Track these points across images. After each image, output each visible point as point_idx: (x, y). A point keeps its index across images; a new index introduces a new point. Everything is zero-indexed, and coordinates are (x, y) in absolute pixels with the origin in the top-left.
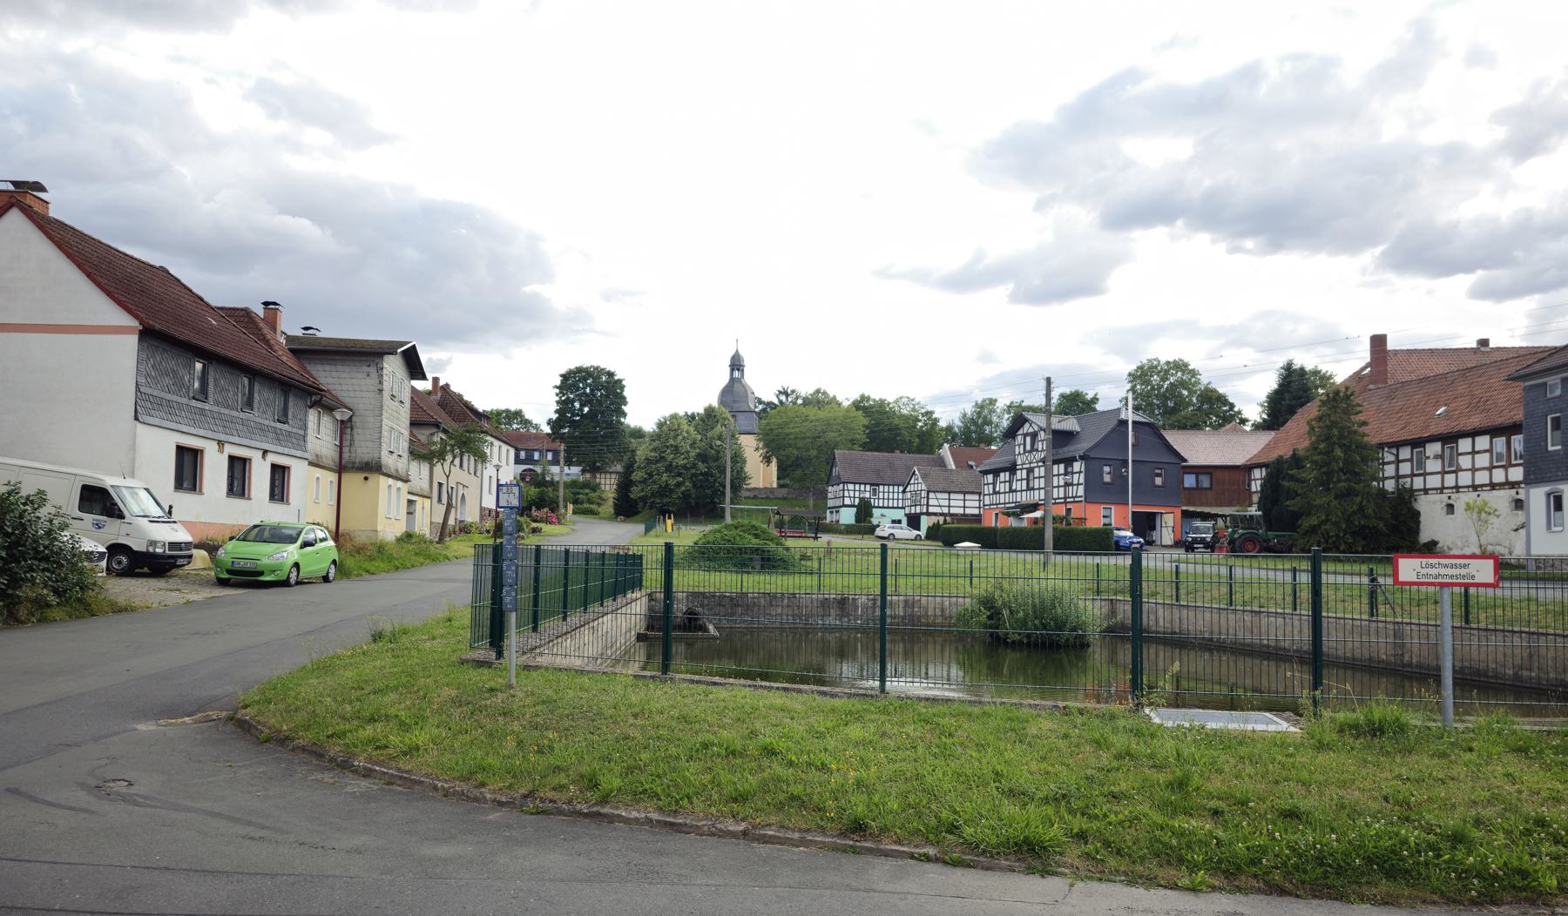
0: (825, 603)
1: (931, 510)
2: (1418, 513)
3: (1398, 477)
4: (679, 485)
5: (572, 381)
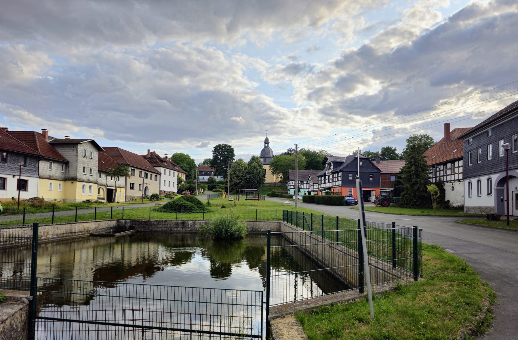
0: (177, 224)
1: (314, 190)
2: (445, 190)
3: (440, 176)
4: (240, 182)
5: (217, 149)
